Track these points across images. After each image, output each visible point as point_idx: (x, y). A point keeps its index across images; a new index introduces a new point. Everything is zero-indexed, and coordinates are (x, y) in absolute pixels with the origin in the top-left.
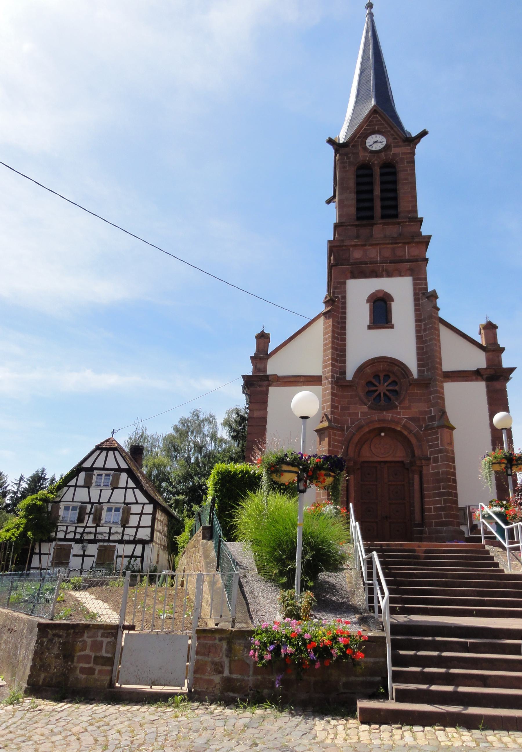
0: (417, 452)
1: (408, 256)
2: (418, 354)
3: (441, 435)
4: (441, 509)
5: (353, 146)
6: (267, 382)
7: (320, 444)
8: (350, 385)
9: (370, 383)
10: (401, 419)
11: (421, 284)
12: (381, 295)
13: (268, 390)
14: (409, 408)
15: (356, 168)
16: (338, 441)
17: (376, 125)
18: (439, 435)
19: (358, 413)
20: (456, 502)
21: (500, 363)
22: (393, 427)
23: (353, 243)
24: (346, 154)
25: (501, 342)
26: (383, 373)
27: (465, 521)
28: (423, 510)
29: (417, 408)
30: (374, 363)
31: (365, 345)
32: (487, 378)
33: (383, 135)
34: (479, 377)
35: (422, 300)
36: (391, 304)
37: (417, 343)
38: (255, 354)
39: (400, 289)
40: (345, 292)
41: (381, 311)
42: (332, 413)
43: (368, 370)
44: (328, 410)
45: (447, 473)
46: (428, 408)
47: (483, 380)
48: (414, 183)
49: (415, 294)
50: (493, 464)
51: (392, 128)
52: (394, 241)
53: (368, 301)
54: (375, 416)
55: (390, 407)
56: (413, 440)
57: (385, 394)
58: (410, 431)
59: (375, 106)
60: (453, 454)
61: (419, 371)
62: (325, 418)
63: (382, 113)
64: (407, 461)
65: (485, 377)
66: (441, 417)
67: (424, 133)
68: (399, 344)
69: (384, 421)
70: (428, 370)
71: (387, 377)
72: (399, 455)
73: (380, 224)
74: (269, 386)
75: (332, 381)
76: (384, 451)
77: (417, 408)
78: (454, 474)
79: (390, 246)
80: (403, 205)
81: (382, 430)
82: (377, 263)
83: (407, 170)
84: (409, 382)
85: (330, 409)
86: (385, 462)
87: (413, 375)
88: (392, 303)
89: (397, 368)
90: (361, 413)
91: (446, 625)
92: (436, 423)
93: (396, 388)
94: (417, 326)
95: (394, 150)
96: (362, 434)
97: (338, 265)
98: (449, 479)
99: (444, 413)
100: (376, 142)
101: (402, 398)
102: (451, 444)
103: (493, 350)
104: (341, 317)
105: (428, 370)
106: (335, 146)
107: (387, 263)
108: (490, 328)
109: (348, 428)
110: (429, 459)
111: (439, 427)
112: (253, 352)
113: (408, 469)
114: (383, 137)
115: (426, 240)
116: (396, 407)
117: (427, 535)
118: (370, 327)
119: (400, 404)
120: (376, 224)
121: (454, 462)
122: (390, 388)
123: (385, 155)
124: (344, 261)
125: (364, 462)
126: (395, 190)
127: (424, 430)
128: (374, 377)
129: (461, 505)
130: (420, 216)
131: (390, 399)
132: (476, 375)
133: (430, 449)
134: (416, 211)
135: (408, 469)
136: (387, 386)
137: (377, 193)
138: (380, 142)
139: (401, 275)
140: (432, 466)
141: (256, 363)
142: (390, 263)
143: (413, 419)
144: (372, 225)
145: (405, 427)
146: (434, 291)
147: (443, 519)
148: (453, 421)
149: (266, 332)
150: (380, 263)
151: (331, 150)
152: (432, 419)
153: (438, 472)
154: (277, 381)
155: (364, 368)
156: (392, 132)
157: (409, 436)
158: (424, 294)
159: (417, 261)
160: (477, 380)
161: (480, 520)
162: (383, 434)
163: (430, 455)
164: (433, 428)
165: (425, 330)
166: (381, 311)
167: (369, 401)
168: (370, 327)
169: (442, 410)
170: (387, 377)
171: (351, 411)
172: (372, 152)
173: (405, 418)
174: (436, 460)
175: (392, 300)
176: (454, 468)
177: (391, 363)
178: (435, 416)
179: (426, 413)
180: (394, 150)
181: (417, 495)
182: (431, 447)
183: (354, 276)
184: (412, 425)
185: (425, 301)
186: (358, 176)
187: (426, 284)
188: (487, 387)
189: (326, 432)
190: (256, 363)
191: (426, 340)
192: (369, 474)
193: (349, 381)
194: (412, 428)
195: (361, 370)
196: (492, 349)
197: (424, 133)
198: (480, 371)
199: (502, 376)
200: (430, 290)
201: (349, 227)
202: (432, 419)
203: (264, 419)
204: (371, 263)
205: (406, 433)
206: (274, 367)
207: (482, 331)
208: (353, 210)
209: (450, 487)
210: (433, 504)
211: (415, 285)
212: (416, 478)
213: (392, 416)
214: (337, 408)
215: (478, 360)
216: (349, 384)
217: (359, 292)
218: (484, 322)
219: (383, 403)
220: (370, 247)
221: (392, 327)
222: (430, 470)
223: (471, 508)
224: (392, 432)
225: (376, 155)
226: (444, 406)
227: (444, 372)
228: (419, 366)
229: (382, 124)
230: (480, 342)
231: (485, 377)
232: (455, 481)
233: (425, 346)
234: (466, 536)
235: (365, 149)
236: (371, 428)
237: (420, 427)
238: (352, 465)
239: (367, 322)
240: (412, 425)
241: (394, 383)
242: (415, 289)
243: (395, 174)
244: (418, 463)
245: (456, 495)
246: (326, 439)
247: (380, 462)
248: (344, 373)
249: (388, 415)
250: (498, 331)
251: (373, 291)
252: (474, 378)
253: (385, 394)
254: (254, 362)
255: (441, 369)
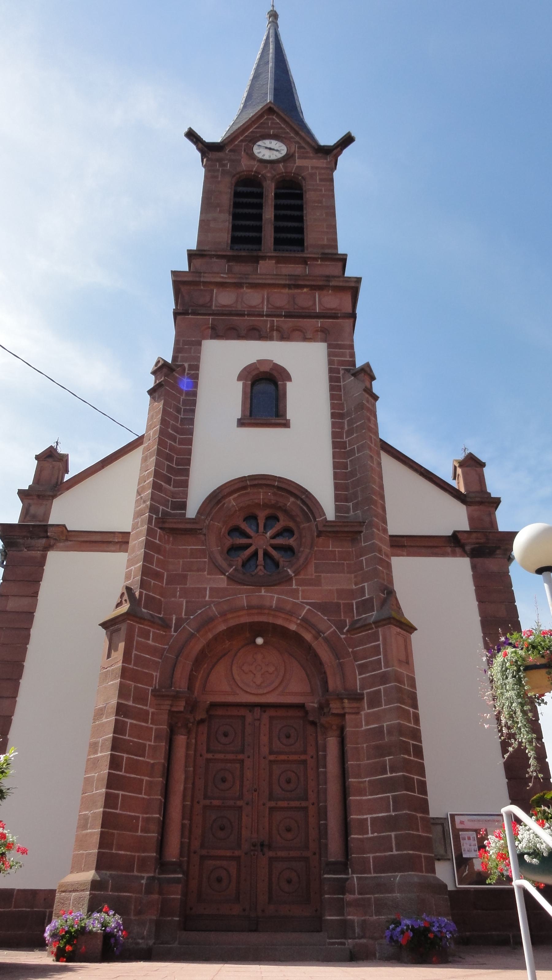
0: (334, 683)
1: (320, 308)
2: (336, 476)
3: (385, 639)
4: (390, 823)
5: (231, 151)
6: (44, 541)
7: (109, 656)
8: (191, 530)
9: (235, 530)
10: (300, 606)
11: (343, 355)
12: (265, 368)
13: (44, 557)
14: (317, 582)
15: (234, 180)
16: (153, 651)
17: (271, 128)
18: (380, 642)
19: (206, 589)
20: (424, 806)
21: (493, 523)
22: (279, 622)
23: (219, 280)
24: (220, 160)
25: (494, 487)
26: (264, 512)
27: (446, 851)
28: (346, 827)
29: (333, 584)
30: (244, 488)
31: (226, 451)
32: (473, 550)
33: (282, 141)
34: (458, 550)
35: (344, 381)
36: (285, 386)
37: (335, 455)
38: (30, 486)
39: (304, 363)
40: (198, 359)
41: (265, 397)
42: (143, 584)
43: (232, 502)
44: (135, 581)
45: (401, 730)
46: (356, 584)
47: (465, 554)
48: (332, 208)
49: (331, 370)
50: (528, 668)
51: (297, 133)
52: (295, 284)
53: (240, 378)
54: (243, 597)
55: (276, 577)
56: (325, 654)
57: (266, 554)
58: (318, 634)
59: (270, 102)
60: (414, 686)
61: (338, 509)
62: (126, 597)
63: (277, 106)
64: (312, 704)
65: (468, 548)
66: (384, 602)
67: (348, 140)
68: (301, 454)
69: (260, 609)
70: (356, 507)
71: (272, 518)
72: (295, 688)
73: (271, 258)
74: (48, 548)
75: (150, 518)
76: (257, 679)
77: (333, 584)
78: (416, 735)
79: (286, 291)
80: (312, 236)
81: (258, 629)
82: (262, 316)
83: (321, 190)
84: (317, 528)
85: (139, 578)
86: (264, 707)
87: (324, 514)
88: (288, 384)
89: (292, 499)
90: (211, 589)
91: (425, 965)
92: (374, 615)
93: (291, 541)
94: (334, 425)
95: (299, 162)
96: (210, 636)
97: (188, 314)
98: (406, 747)
99: (390, 593)
100: (269, 150)
101: (301, 560)
102: (407, 661)
103: (480, 502)
104: (184, 400)
105: (356, 507)
106: (200, 145)
107: (280, 316)
108: (472, 464)
109: (180, 622)
110: (358, 698)
111: (378, 623)
112: (27, 481)
113: (314, 723)
114: (281, 144)
115: (353, 284)
116: (289, 580)
117: (357, 896)
118: (241, 423)
119: (297, 573)
120: (264, 258)
121: (415, 706)
122: (279, 541)
123: (283, 166)
124: (200, 305)
125: (214, 705)
126: (300, 219)
127: (348, 631)
128: (246, 519)
129: (435, 812)
130: (341, 250)
131: (277, 565)
132: (453, 544)
133: (360, 674)
134: (336, 247)
135: (314, 723)
136: (273, 537)
137: (267, 217)
138: (277, 150)
139: (305, 339)
140: (367, 715)
141: (30, 505)
142: (286, 316)
143: (323, 607)
144: (256, 260)
145: (306, 622)
146: (368, 365)
147: (395, 852)
148: (410, 614)
149: (61, 450)
150: (267, 316)
151: (194, 153)
152: (366, 606)
153: (380, 730)
154: (67, 540)
155: (224, 497)
156: (297, 139)
157: (314, 644)
158: (348, 371)
159: (335, 317)
160: (454, 554)
161: (510, 880)
162: (260, 641)
163: (363, 688)
164: (366, 627)
165: (350, 433)
166: (265, 397)
167: (230, 566)
168: (241, 423)
169: (386, 588)
170: (272, 518)
171: (189, 585)
172: (262, 161)
173: (307, 604)
174: (375, 701)
175: (288, 378)
176: (417, 720)
177: (279, 488)
178: (371, 600)
179: (352, 594)
180: (299, 162)
181: (333, 788)
182: (363, 668)
183: (217, 335)
184: (324, 622)
185: (353, 393)
186: (237, 194)
187: (353, 355)
188: (474, 567)
189: (124, 627)
190: (30, 505)
191: (353, 450)
192: (226, 735)
193: (191, 521)
194: (322, 627)
195: (216, 498)
196: (478, 499)
197: (348, 140)
198: (459, 535)
199: (499, 548)
200: (359, 363)
201: (214, 260)
202: (366, 606)
203: (28, 616)
204: (249, 315)
205: (308, 637)
206: (64, 512)
207: (459, 471)
208: (225, 237)
209: (407, 766)
210: (370, 810)
211: (330, 355)
212: (332, 743)
213: (279, 599)
214: (157, 576)
215: (454, 518)
216: (188, 526)
217: (225, 361)
218: (461, 457)
219: (260, 570)
220: (249, 290)
221: (286, 424)
222: (362, 723)
223: (457, 819)
224: (278, 634)
225: (269, 165)
226: (391, 581)
227: (391, 536)
228: (337, 498)
229: (282, 128)
230: (457, 487)
231: (468, 548)
232: (419, 752)
233: (350, 461)
234: (450, 888)
235: (252, 156)
236: (232, 623)
237: (340, 625)
238: (182, 709)
239: (237, 412)
240: (324, 622)
241: (288, 531)
242: (330, 362)
243: (300, 196)
244: (335, 707)
245: (423, 787)
246: (122, 646)
247: (251, 706)
248: (183, 506)
249: (270, 597)
250: (485, 470)
251: (253, 360)
252: (449, 550)
253: (266, 554)
254: (27, 501)
255: (385, 530)
